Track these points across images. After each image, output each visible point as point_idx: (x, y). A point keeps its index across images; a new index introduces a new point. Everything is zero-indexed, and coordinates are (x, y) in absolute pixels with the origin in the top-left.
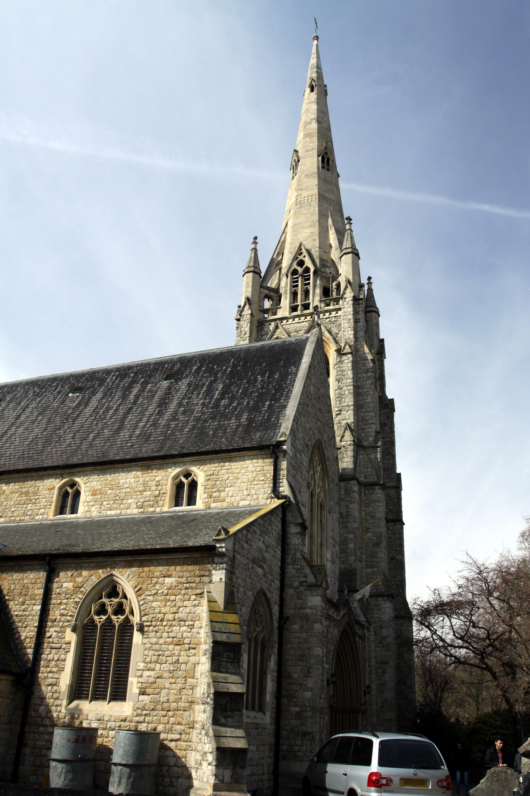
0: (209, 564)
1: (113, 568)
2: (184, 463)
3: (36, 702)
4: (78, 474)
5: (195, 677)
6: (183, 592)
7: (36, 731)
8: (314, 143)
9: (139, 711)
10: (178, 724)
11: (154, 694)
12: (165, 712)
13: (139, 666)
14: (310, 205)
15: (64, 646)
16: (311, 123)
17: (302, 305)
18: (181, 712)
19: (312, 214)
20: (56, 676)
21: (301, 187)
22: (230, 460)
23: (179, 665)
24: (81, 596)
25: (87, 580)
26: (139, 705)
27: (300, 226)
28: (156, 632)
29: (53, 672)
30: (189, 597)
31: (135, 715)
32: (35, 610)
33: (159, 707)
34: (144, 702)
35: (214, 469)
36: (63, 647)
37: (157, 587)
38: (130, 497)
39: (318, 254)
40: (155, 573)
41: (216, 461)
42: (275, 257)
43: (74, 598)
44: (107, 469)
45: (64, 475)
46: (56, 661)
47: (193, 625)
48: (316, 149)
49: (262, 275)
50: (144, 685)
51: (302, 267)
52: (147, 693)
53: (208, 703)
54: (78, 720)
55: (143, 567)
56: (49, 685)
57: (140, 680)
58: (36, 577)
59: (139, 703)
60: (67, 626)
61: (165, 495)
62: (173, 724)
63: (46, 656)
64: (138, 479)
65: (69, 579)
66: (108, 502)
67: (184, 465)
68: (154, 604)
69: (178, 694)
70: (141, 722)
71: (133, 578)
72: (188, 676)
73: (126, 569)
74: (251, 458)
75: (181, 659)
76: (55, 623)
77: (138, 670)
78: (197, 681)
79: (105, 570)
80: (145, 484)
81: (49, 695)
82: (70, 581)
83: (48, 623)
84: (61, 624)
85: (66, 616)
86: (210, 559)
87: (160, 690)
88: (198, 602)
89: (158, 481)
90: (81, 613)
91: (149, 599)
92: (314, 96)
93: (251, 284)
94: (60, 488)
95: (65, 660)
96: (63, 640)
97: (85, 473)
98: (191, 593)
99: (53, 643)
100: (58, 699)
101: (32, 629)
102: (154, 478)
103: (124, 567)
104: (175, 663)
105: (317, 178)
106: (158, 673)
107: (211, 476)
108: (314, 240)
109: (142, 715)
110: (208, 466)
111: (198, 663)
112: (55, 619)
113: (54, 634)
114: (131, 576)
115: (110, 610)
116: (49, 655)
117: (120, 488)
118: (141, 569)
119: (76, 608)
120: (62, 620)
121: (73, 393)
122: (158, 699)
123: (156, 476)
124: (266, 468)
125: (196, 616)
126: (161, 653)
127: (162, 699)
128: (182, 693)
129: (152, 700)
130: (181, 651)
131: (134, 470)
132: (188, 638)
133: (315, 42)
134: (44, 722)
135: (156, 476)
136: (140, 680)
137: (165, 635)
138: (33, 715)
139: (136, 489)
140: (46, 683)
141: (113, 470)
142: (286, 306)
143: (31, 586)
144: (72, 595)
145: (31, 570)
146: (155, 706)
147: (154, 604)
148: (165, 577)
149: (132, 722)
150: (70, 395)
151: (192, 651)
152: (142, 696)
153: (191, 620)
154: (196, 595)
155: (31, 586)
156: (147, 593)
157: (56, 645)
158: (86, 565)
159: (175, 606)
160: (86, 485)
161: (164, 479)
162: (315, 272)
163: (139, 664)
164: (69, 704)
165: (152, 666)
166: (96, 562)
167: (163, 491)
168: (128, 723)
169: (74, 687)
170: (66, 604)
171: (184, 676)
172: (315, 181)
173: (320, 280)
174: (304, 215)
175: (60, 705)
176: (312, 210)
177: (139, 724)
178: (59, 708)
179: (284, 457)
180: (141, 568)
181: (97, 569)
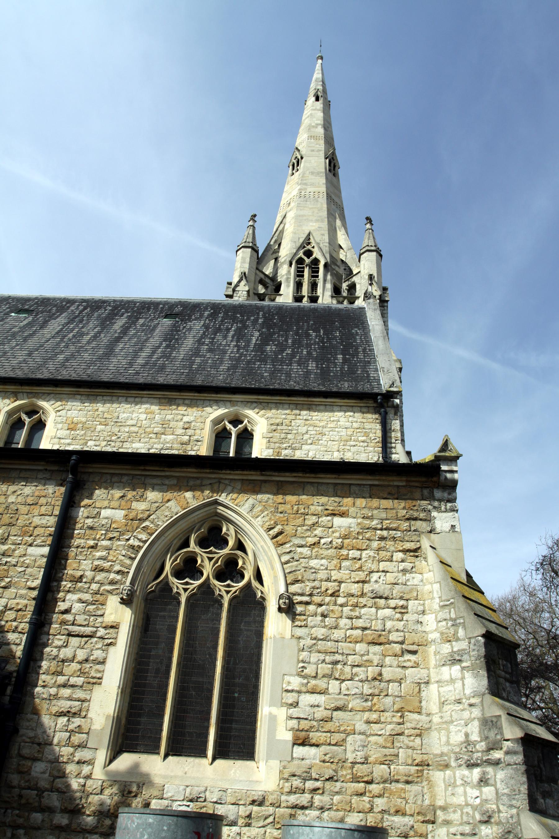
0: (423, 499)
1: (219, 491)
2: (233, 403)
3: (26, 752)
4: (46, 396)
5: (424, 711)
6: (375, 544)
7: (21, 821)
8: (321, 145)
9: (297, 782)
10: (397, 812)
11: (330, 744)
12: (362, 785)
13: (289, 683)
14: (317, 201)
15: (101, 632)
16: (317, 128)
17: (308, 296)
18: (400, 786)
19: (320, 210)
20: (80, 694)
21: (305, 181)
22: (310, 408)
23: (383, 684)
24: (144, 537)
25: (158, 508)
26: (292, 768)
27: (304, 218)
28: (324, 616)
29: (73, 686)
30: (389, 554)
31: (287, 789)
32: (30, 555)
33: (345, 773)
34: (308, 762)
35: (284, 416)
36: (99, 634)
37: (318, 531)
38: (138, 439)
39: (327, 249)
40: (312, 507)
41: (286, 406)
42: (272, 243)
43: (128, 540)
44: (97, 395)
45: (20, 395)
46: (80, 663)
47: (406, 608)
48: (323, 152)
49: (260, 254)
50: (304, 725)
51: (309, 258)
52: (314, 741)
53: (496, 763)
54: (138, 799)
55: (285, 494)
56: (62, 714)
57: (294, 712)
58: (37, 493)
59: (296, 762)
60: (110, 592)
61: (199, 443)
62: (383, 812)
63: (55, 650)
64: (154, 416)
65: (114, 504)
66: (97, 443)
67: (234, 406)
68: (314, 563)
69: (389, 745)
70: (303, 808)
71: (262, 511)
72: (407, 708)
73: (246, 496)
74: (342, 408)
75: (387, 673)
76: (80, 585)
77: (287, 691)
78: (428, 719)
79: (198, 493)
80: (164, 424)
81: (59, 737)
82: (119, 508)
83: (64, 583)
84: (94, 586)
85: (108, 571)
86: (426, 492)
87: (343, 736)
88: (411, 565)
89: (188, 422)
90: (144, 569)
91: (301, 553)
92: (319, 105)
93: (248, 260)
94: (10, 414)
95: (103, 662)
96: (100, 619)
97: (57, 396)
98: (392, 549)
99: (73, 624)
100: (85, 747)
101: (23, 592)
102: (180, 417)
103: (242, 491)
104: (374, 679)
105: (324, 177)
106: (337, 700)
107: (278, 425)
108: (323, 235)
109: (303, 792)
110: (273, 411)
111: (427, 683)
112: (81, 577)
113: (77, 607)
114: (258, 508)
115: (208, 569)
116: (63, 650)
117: (120, 424)
118: (279, 498)
119: (133, 559)
120: (97, 578)
121: (16, 313)
122: (341, 756)
123: (184, 415)
124: (367, 426)
125: (411, 591)
126: (338, 657)
127: (350, 757)
128: (396, 744)
129: (327, 758)
130: (385, 656)
131: (147, 403)
132: (397, 630)
133: (320, 61)
134: (45, 801)
135: (184, 415)
136: (294, 712)
137: (343, 622)
138: (15, 783)
139: (148, 430)
140: (54, 710)
141: (109, 398)
142: (288, 294)
143: (24, 509)
144: (122, 534)
145: (27, 480)
146: (336, 771)
147: (314, 563)
148: (334, 515)
149: (279, 806)
150: (13, 314)
151: (408, 657)
152: (301, 748)
153: (401, 598)
154: (405, 551)
155: (24, 509)
156: (297, 541)
157: (82, 629)
158: (155, 481)
159: (360, 569)
160: (58, 414)
161: (199, 420)
162: (326, 265)
163: (287, 678)
164: (111, 761)
165: (321, 684)
166: (178, 478)
167: (196, 437)
168: (271, 810)
169: (123, 721)
170: (109, 549)
171: (396, 707)
172: (324, 181)
173: (331, 275)
174: (310, 208)
175: (90, 762)
176: (319, 206)
177: (299, 812)
178: (86, 769)
179: (396, 414)
180: (280, 497)
181: (180, 490)
